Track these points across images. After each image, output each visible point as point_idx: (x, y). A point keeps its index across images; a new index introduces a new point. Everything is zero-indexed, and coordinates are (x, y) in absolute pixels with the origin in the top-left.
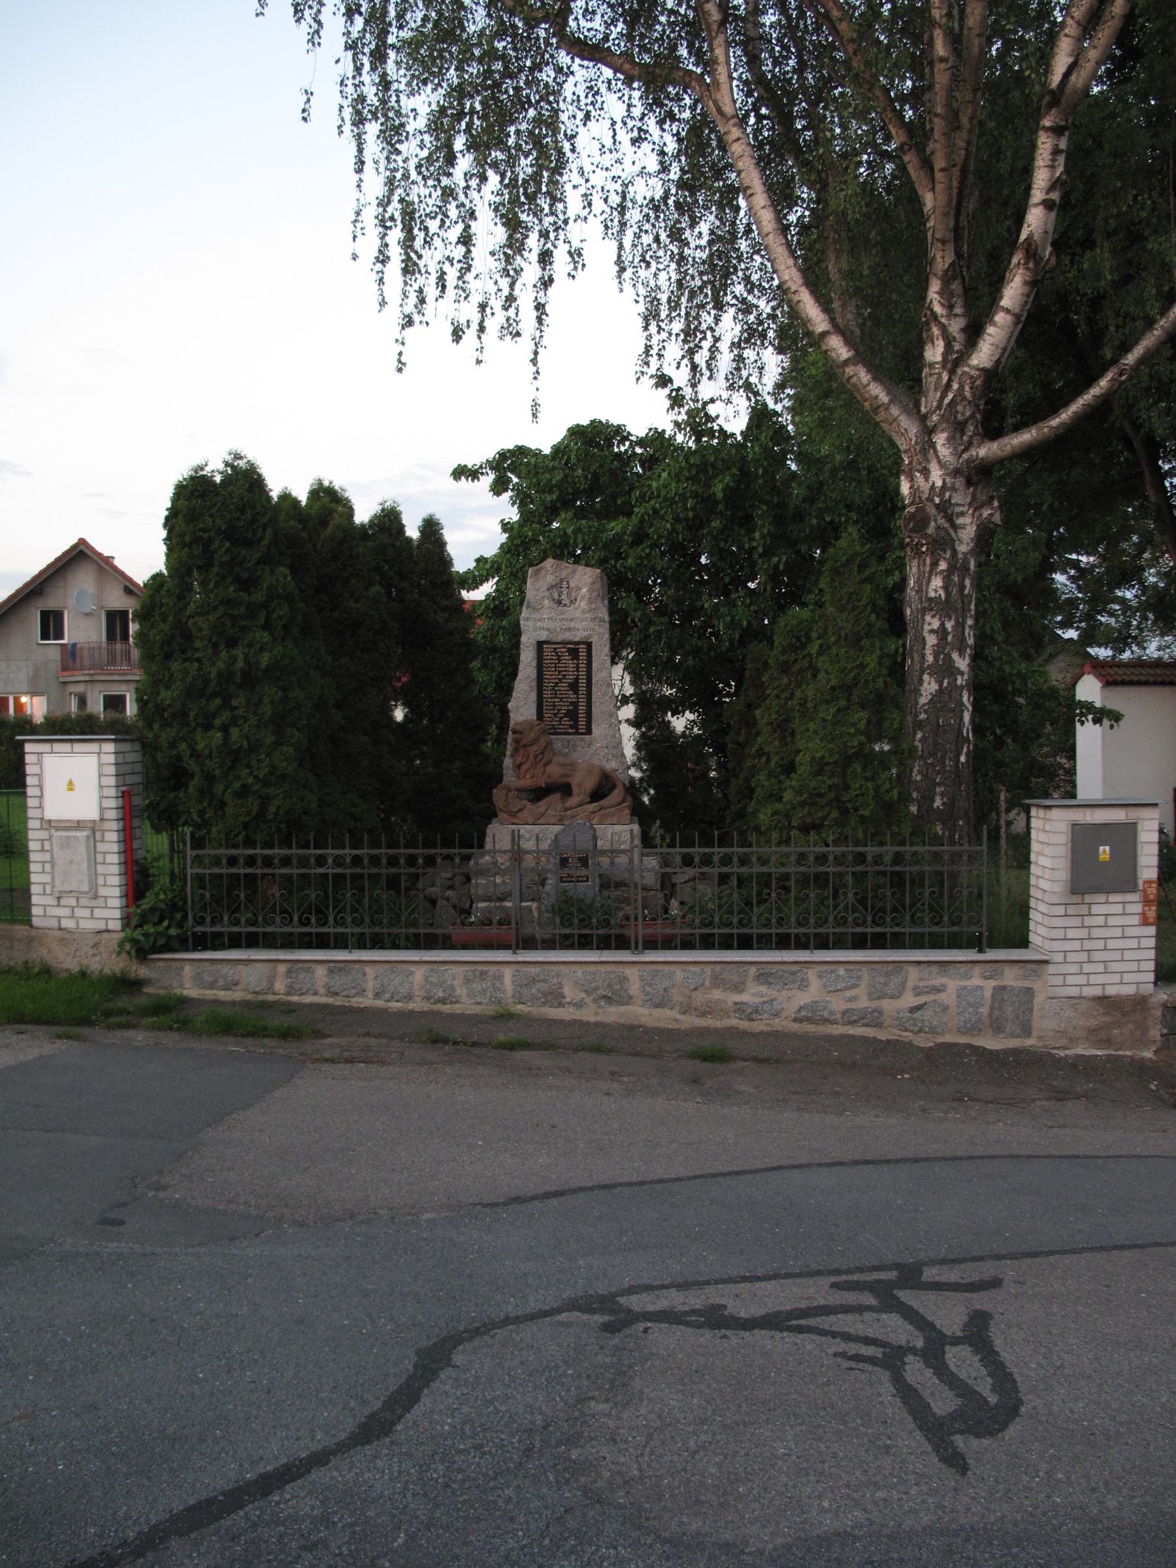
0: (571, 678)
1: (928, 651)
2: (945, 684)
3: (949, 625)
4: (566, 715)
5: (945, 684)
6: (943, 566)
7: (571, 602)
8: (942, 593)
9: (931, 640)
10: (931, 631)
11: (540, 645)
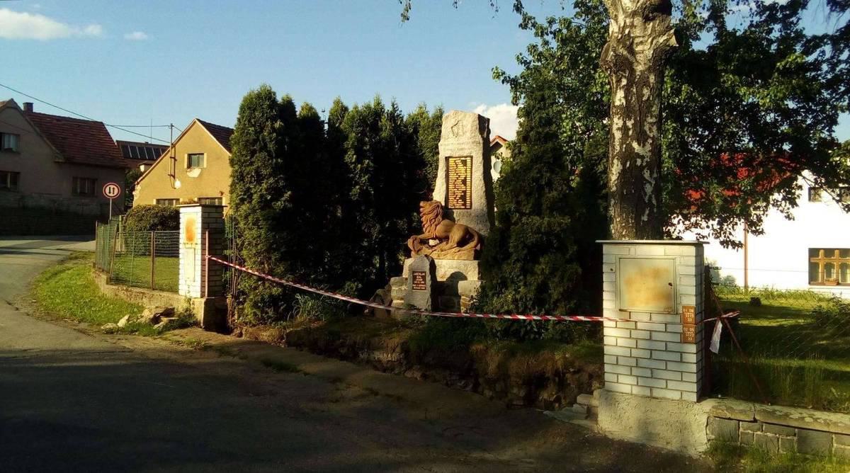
0: (462, 177)
1: (617, 143)
2: (628, 165)
3: (630, 124)
4: (460, 198)
5: (628, 165)
6: (624, 82)
7: (464, 133)
8: (624, 101)
9: (618, 135)
10: (618, 129)
11: (447, 159)
